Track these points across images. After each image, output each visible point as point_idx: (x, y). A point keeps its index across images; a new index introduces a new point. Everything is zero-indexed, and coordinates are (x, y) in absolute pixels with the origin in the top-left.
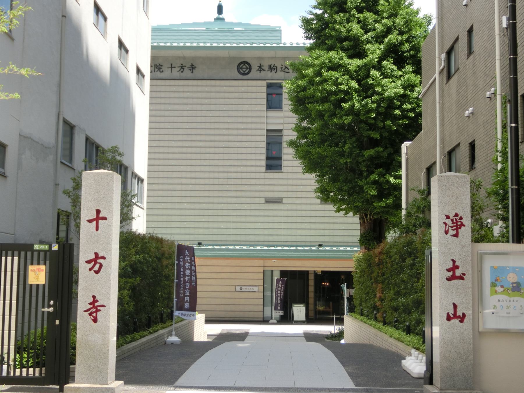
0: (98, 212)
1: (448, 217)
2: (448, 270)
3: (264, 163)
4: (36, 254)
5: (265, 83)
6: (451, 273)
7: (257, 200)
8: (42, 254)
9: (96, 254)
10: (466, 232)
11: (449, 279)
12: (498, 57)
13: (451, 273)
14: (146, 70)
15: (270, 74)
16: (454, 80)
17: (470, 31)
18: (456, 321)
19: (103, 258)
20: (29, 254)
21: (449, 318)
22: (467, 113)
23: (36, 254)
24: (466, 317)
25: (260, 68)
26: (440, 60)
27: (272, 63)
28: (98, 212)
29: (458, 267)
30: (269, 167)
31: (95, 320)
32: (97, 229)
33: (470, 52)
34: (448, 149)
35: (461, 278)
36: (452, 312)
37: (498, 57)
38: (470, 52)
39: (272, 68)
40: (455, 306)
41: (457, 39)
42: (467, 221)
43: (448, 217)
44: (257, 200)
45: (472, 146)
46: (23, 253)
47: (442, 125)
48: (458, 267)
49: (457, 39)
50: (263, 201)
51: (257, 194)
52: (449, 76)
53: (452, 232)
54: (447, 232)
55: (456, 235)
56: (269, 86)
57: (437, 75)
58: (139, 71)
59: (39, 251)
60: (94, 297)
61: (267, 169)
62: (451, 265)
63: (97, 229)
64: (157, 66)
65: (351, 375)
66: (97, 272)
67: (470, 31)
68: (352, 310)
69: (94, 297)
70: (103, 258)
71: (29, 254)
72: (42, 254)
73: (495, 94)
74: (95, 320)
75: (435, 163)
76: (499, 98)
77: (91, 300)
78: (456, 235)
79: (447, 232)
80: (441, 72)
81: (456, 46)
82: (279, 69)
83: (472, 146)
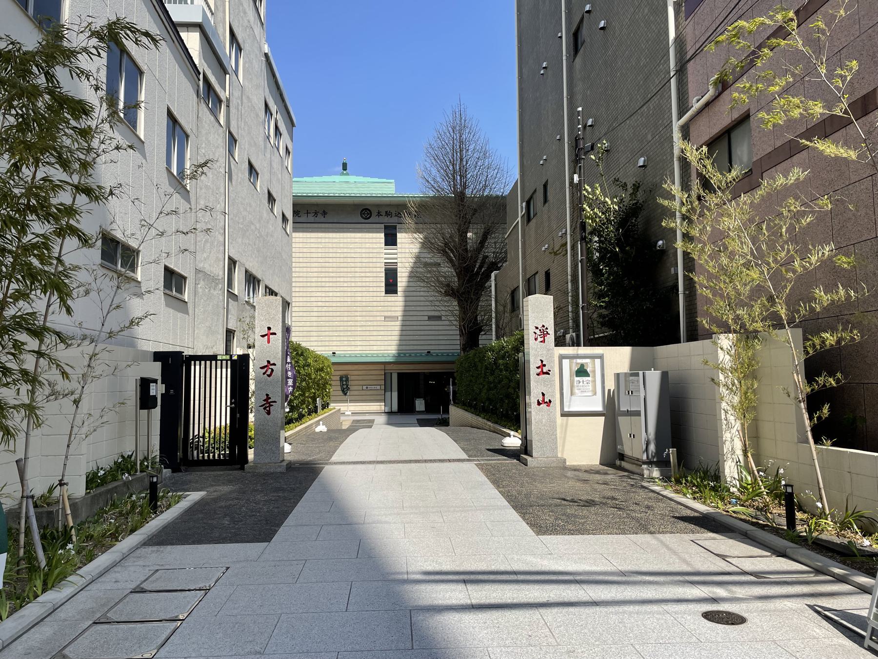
0: (269, 328)
1: (537, 328)
2: (538, 368)
3: (383, 289)
4: (219, 362)
5: (383, 226)
6: (540, 370)
7: (378, 318)
8: (224, 362)
9: (268, 362)
10: (551, 338)
11: (538, 375)
12: (568, 205)
13: (540, 370)
14: (289, 215)
15: (387, 219)
16: (533, 223)
17: (545, 186)
18: (544, 406)
19: (274, 364)
20: (214, 362)
21: (539, 404)
22: (543, 249)
23: (219, 362)
24: (253, 549)
25: (379, 214)
26: (522, 207)
27: (388, 209)
28: (269, 328)
29: (545, 365)
30: (387, 292)
31: (269, 413)
32: (269, 342)
33: (546, 200)
34: (528, 277)
35: (547, 373)
36: (541, 399)
37: (568, 205)
38: (546, 200)
39: (388, 214)
40: (543, 395)
41: (535, 191)
42: (551, 331)
43: (537, 328)
44: (378, 318)
45: (547, 274)
46: (203, 363)
47: (524, 257)
48: (545, 365)
49: (535, 191)
50: (426, 318)
51: (378, 314)
52: (529, 220)
53: (540, 339)
54: (536, 339)
55: (543, 341)
56: (386, 227)
57: (519, 219)
58: (283, 215)
59: (222, 361)
60: (267, 395)
61: (386, 293)
62: (540, 364)
63: (269, 342)
64: (296, 213)
65: (463, 449)
66: (269, 376)
67: (545, 186)
68: (456, 403)
69: (267, 395)
70: (274, 364)
71: (214, 362)
72: (224, 362)
73: (566, 233)
74: (269, 413)
75: (518, 287)
76: (569, 236)
77: (265, 397)
78: (543, 341)
79: (536, 339)
80: (523, 217)
81: (534, 196)
82: (394, 215)
83: (547, 274)
